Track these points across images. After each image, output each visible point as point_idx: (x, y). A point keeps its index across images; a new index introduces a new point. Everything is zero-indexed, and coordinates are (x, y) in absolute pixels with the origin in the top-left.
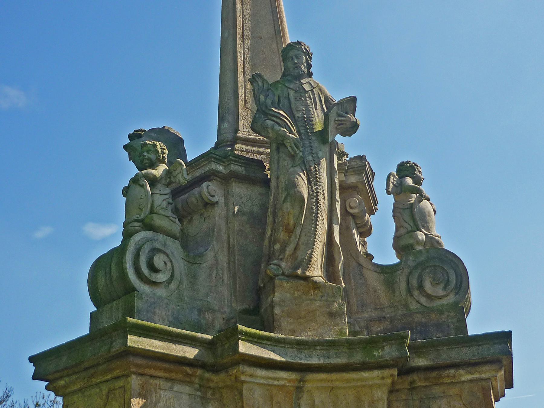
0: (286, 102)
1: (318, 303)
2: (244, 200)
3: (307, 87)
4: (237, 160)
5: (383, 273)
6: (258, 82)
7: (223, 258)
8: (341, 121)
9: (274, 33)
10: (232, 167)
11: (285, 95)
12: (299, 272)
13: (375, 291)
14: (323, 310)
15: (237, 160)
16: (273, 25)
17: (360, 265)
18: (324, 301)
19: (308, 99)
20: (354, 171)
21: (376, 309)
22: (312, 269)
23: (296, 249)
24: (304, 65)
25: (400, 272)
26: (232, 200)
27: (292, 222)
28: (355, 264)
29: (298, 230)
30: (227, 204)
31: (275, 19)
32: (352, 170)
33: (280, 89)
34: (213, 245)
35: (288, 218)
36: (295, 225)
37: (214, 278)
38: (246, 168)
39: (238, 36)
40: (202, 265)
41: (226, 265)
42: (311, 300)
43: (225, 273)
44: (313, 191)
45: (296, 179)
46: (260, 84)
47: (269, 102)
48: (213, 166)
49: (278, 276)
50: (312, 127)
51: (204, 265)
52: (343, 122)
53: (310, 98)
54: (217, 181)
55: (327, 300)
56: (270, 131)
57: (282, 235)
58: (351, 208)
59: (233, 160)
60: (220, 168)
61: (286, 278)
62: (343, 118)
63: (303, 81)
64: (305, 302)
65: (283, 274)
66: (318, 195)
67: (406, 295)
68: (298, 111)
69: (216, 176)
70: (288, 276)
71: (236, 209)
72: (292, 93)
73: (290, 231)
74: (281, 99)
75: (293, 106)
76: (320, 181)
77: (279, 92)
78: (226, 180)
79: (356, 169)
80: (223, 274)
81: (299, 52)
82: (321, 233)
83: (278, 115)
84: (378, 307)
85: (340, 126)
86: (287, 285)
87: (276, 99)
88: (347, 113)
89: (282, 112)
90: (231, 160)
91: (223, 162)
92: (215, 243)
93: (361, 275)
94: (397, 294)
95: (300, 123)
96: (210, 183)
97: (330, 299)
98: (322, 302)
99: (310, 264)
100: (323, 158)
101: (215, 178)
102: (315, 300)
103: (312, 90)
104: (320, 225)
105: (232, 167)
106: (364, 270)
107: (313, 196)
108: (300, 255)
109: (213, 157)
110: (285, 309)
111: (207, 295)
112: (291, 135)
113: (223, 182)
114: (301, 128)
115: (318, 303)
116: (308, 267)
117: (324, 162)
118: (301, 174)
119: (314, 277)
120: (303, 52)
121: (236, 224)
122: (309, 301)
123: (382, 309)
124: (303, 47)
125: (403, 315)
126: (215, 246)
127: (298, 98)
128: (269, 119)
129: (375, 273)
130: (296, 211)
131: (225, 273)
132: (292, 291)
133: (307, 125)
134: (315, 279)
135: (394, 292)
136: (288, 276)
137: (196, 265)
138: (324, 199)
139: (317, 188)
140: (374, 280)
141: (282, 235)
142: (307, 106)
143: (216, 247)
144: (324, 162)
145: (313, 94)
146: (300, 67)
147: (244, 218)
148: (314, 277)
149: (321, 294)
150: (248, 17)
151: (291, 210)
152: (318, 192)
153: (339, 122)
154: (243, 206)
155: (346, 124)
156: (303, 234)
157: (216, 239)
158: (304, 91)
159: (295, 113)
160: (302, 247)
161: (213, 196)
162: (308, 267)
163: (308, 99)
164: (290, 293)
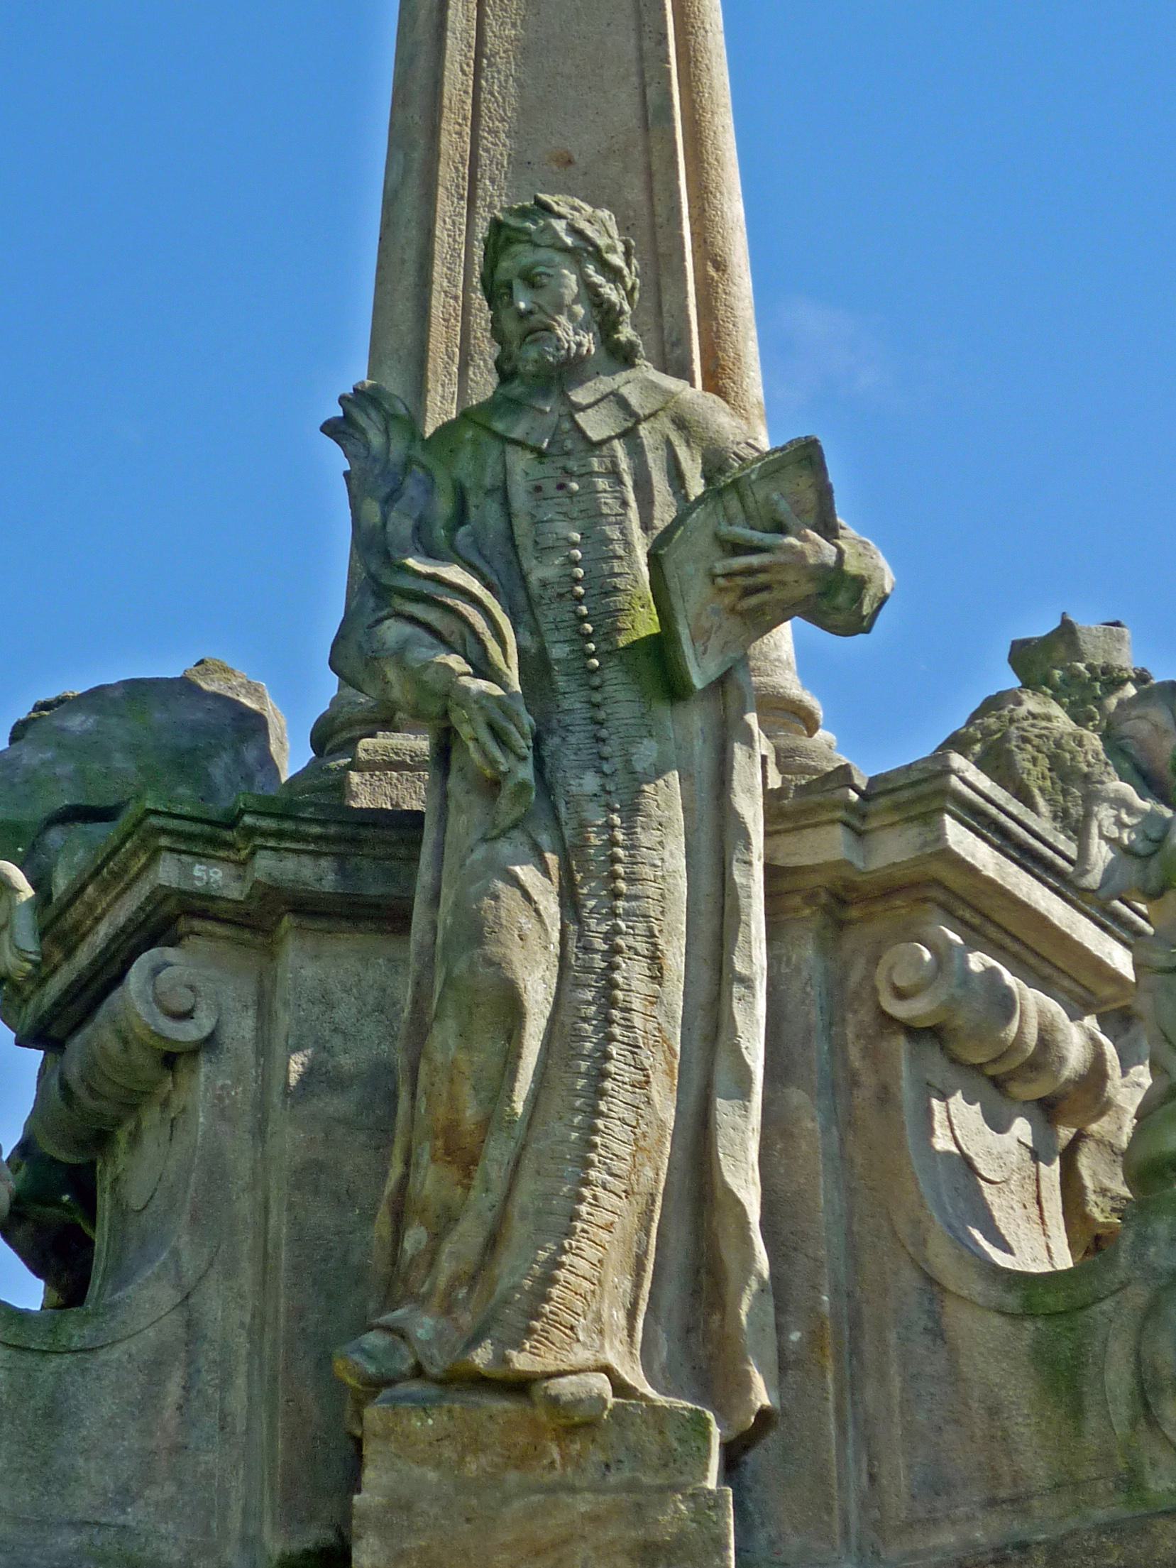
0: (492, 509)
1: (583, 1504)
2: (345, 1012)
3: (597, 425)
4: (288, 825)
5: (1034, 1316)
6: (363, 432)
7: (225, 1312)
8: (750, 571)
9: (634, 123)
10: (265, 865)
11: (488, 481)
12: (482, 1357)
13: (994, 1412)
14: (612, 1533)
15: (288, 825)
16: (634, 80)
17: (930, 1280)
18: (616, 1489)
19: (602, 483)
20: (897, 807)
21: (992, 1503)
22: (556, 1334)
23: (493, 1243)
24: (572, 317)
25: (1107, 1305)
26: (285, 1020)
27: (470, 1113)
28: (908, 1277)
29: (497, 1153)
30: (263, 1047)
31: (648, 44)
32: (884, 802)
33: (467, 451)
34: (175, 1253)
35: (453, 1098)
36: (486, 1125)
37: (169, 1413)
38: (341, 858)
39: (446, 173)
40: (103, 1356)
41: (241, 1343)
42: (551, 1490)
43: (240, 1381)
44: (588, 949)
45: (488, 902)
46: (376, 439)
47: (401, 526)
48: (167, 872)
49: (389, 1383)
50: (609, 620)
51: (117, 1353)
52: (762, 578)
53: (614, 474)
54: (211, 936)
55: (632, 1486)
56: (392, 674)
57: (432, 1181)
58: (901, 994)
59: (265, 834)
60: (211, 875)
61: (433, 1391)
62: (755, 560)
63: (580, 396)
64: (517, 1505)
65: (418, 1372)
66: (613, 967)
67: (1133, 1423)
68: (543, 551)
69: (204, 915)
70: (440, 1382)
71: (296, 1065)
72: (520, 462)
73: (463, 1158)
74: (472, 500)
75: (522, 526)
76: (637, 889)
77: (464, 466)
78: (256, 921)
79: (905, 795)
80: (225, 1384)
81: (543, 254)
82: (624, 1151)
83: (429, 588)
84: (1003, 1493)
85: (753, 601)
86: (422, 1424)
87: (444, 506)
88: (781, 529)
89: (454, 574)
90: (251, 832)
91: (229, 845)
92: (183, 1241)
93: (937, 1333)
94: (1092, 1422)
95: (550, 615)
96: (170, 953)
97: (647, 1479)
98: (609, 1498)
99: (538, 1316)
100: (660, 772)
101: (197, 924)
102: (572, 1490)
103: (630, 435)
104: (620, 1110)
105: (265, 865)
106: (950, 1305)
107: (588, 969)
108: (513, 1272)
109: (163, 831)
110: (411, 1543)
111: (125, 1496)
112: (483, 685)
113: (247, 935)
114: (550, 637)
115: (583, 1504)
116: (530, 1331)
117: (667, 799)
118: (526, 873)
119: (561, 1374)
120: (565, 249)
121: (290, 1139)
122: (536, 1498)
123: (1019, 1503)
124: (560, 226)
125: (1111, 1527)
126: (185, 1256)
127: (550, 487)
128: (399, 615)
129: (997, 1321)
130: (486, 1053)
131: (240, 1381)
132: (448, 1452)
133: (583, 619)
134: (565, 1387)
135: (1077, 1412)
136: (440, 1382)
137: (68, 1358)
138: (657, 976)
139: (616, 931)
140: (991, 1350)
141: (432, 1181)
142: (594, 516)
143: (191, 1264)
144: (667, 799)
145: (636, 451)
146: (549, 329)
147: (338, 1105)
148: (561, 1374)
149: (600, 1457)
150: (504, 64)
151: (462, 1057)
152: (616, 950)
153: (741, 581)
154: (337, 1041)
155: (783, 583)
156: (529, 1165)
157: (194, 1219)
158: (581, 446)
159: (529, 563)
160: (519, 1230)
161: (187, 1015)
162: (530, 1331)
163: (602, 483)
164: (438, 1465)
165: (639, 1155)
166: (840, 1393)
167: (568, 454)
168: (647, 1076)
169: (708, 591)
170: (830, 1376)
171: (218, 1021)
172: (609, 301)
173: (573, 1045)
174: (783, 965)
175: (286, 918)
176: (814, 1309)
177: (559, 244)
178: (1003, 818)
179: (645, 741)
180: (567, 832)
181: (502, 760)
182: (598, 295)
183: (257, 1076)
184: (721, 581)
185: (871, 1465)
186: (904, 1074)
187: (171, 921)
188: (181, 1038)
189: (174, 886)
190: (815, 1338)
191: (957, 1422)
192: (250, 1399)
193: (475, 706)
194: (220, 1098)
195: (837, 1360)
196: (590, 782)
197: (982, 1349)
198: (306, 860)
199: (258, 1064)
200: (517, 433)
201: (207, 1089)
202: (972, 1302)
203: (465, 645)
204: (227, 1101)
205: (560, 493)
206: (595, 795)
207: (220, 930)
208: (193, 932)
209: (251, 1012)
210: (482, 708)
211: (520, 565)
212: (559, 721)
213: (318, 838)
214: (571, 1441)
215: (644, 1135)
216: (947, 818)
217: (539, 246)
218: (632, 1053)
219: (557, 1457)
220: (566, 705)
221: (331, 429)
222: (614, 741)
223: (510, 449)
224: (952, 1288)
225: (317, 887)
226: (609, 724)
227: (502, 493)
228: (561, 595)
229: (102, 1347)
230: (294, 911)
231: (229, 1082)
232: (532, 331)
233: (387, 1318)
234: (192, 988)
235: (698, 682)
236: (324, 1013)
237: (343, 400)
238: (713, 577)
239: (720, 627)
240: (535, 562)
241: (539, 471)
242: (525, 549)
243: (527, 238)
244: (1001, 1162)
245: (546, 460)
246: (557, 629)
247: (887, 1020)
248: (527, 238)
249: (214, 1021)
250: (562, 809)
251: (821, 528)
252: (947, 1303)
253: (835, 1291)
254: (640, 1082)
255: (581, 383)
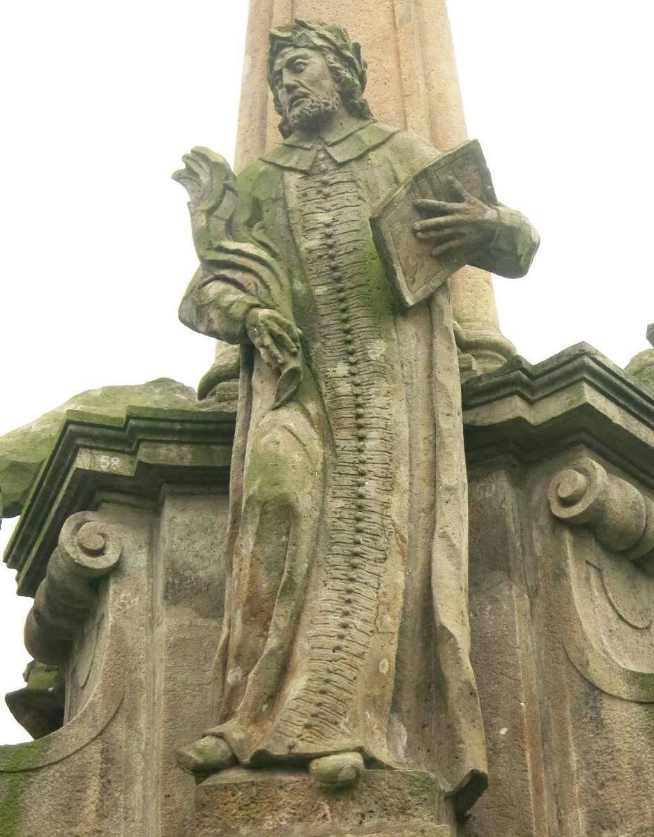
8: (438, 227)
81: (300, 52)
88: (459, 198)
101: (106, 496)
128: (217, 278)
158: (331, 167)
159: (300, 239)
161: (99, 552)
165: (381, 607)
166: (536, 767)
167: (324, 172)
168: (386, 555)
169: (413, 242)
170: (528, 755)
171: (121, 556)
172: (346, 78)
173: (333, 536)
174: (487, 493)
175: (163, 487)
176: (515, 713)
177: (310, 45)
178: (624, 387)
179: (377, 341)
180: (326, 401)
181: (280, 356)
182: (338, 74)
183: (149, 590)
184: (419, 234)
185: (559, 814)
186: (569, 556)
187: (91, 495)
188: (96, 567)
189: (87, 468)
190: (516, 732)
191: (614, 779)
192: (144, 798)
193: (262, 325)
194: (123, 605)
195: (533, 746)
196: (342, 369)
197: (628, 729)
198: (172, 447)
199: (149, 583)
200: (291, 164)
201: (114, 600)
202: (622, 699)
203: (257, 290)
204: (128, 607)
205: (319, 196)
206: (344, 377)
207: (120, 498)
208: (104, 501)
209: (144, 550)
210: (266, 325)
211: (294, 240)
212: (320, 333)
213: (180, 432)
214: (337, 800)
215: (384, 594)
216: (585, 385)
217: (299, 47)
218: (374, 539)
219: (327, 811)
220: (324, 322)
221: (178, 177)
222: (357, 343)
223: (286, 174)
224: (605, 688)
225: (179, 463)
226: (353, 332)
227: (281, 199)
228: (320, 257)
229: (43, 767)
230: (168, 482)
231: (129, 594)
232: (296, 98)
233: (218, 729)
234: (103, 535)
235: (410, 301)
236: (189, 545)
237: (186, 157)
238: (415, 232)
239: (423, 265)
240: (303, 238)
241: (305, 184)
242: (297, 232)
243: (290, 43)
244: (643, 615)
245: (309, 178)
246: (318, 277)
247: (558, 523)
248: (290, 43)
249: (117, 556)
250: (323, 387)
251: (485, 198)
252: (605, 700)
253: (531, 700)
254: (380, 559)
255: (330, 131)
